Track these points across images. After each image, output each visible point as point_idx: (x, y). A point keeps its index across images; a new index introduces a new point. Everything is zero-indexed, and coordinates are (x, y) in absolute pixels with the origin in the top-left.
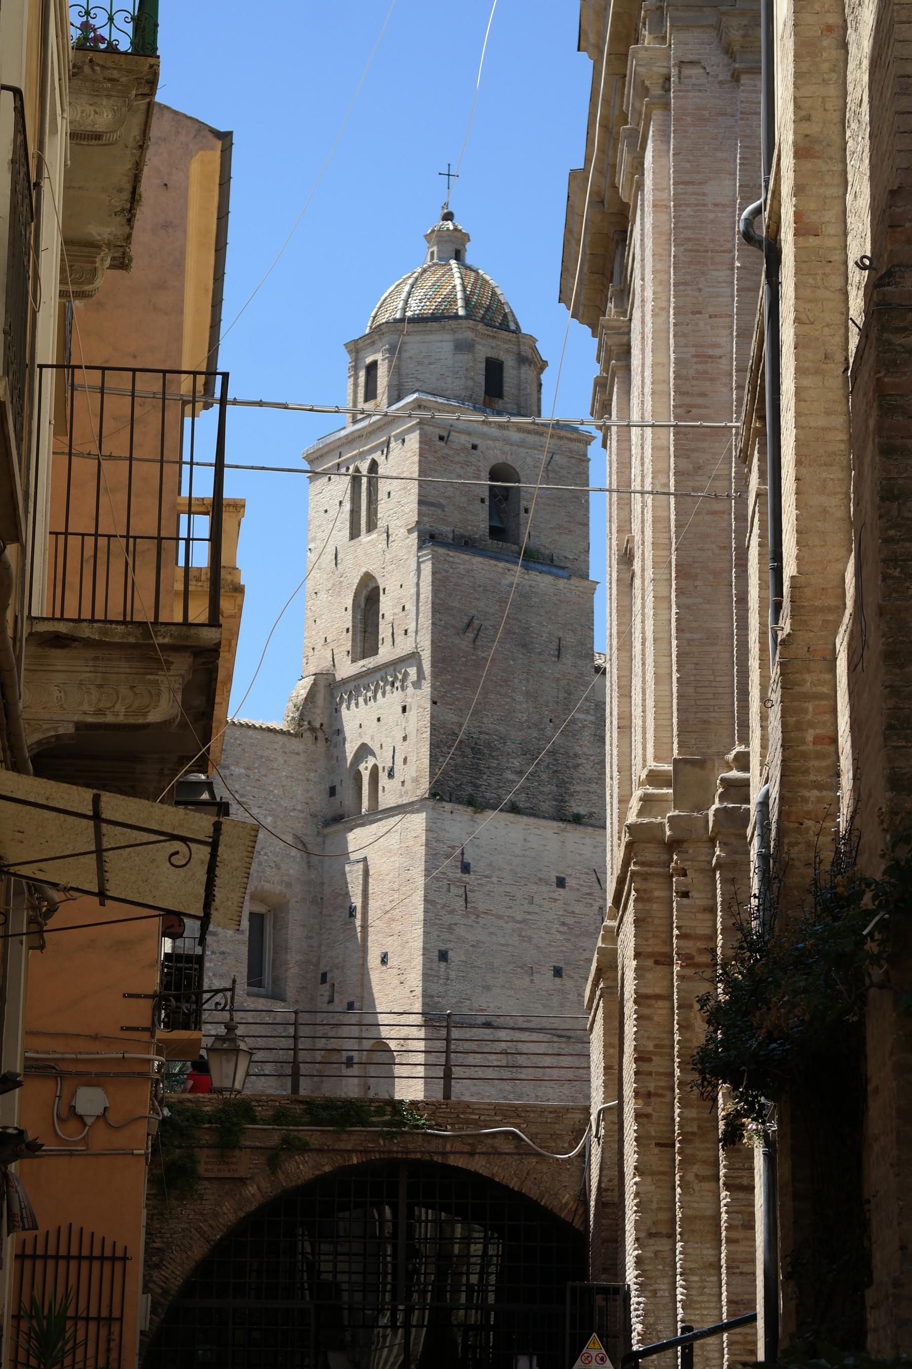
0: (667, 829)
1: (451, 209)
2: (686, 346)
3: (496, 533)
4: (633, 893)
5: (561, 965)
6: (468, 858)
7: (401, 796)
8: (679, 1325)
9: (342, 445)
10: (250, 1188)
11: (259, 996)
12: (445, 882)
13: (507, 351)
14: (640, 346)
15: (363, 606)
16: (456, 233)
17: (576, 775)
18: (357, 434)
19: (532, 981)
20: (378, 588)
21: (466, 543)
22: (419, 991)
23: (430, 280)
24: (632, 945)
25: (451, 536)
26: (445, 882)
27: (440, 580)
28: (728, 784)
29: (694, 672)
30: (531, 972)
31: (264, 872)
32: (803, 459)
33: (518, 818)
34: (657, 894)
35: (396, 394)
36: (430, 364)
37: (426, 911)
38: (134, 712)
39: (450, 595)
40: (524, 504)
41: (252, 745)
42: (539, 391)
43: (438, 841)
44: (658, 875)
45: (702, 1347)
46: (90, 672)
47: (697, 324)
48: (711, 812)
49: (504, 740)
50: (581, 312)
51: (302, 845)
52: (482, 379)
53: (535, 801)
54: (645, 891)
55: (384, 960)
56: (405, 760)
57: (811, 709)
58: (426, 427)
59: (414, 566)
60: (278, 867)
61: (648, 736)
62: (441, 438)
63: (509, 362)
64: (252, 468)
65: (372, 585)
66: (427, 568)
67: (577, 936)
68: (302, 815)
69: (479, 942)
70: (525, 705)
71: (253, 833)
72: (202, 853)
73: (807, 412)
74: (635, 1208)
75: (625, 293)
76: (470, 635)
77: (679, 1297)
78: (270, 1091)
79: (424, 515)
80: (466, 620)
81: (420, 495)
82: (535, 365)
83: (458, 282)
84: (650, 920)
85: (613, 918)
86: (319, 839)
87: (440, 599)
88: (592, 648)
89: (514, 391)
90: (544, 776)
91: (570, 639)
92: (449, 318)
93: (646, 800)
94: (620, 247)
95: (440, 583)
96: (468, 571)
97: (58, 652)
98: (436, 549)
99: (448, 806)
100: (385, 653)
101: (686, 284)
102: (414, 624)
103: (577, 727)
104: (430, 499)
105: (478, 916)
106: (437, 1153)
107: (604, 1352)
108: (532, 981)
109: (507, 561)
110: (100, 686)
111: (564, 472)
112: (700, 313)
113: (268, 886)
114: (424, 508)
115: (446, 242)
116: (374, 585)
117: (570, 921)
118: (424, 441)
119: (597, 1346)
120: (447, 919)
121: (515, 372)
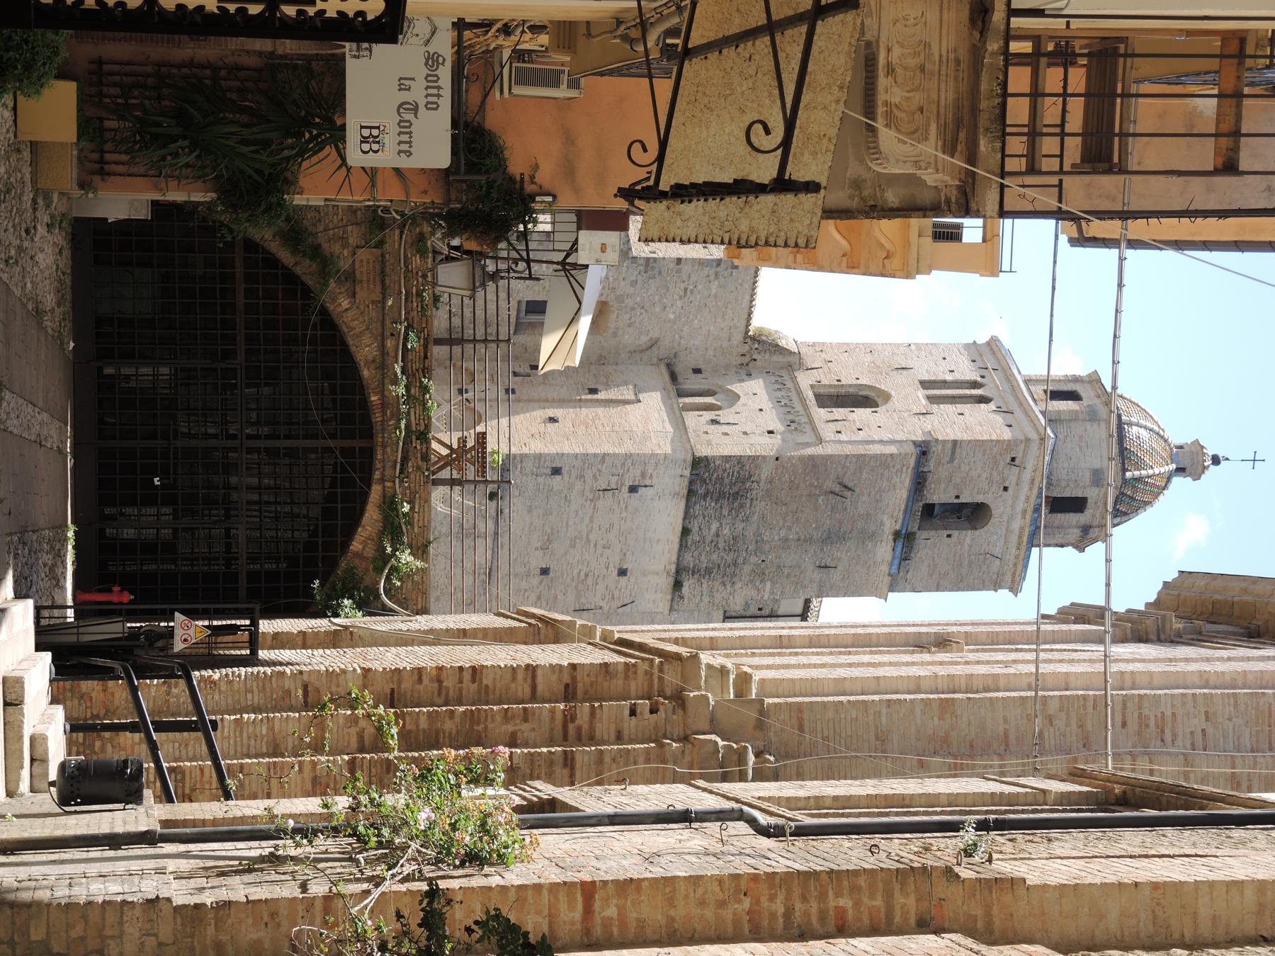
0: (695, 693)
1: (1223, 463)
2: (1173, 706)
3: (929, 510)
4: (633, 661)
5: (551, 574)
6: (642, 491)
7: (694, 431)
8: (219, 717)
9: (1004, 371)
10: (346, 302)
11: (518, 311)
12: (621, 472)
13: (1094, 516)
14: (1161, 656)
15: (860, 393)
16: (1200, 468)
17: (717, 584)
18: (1015, 384)
19: (537, 549)
20: (877, 406)
21: (919, 483)
22: (526, 450)
23: (1158, 446)
24: (583, 660)
25: (925, 470)
26: (621, 472)
27: (886, 461)
28: (741, 757)
29: (849, 718)
30: (544, 548)
31: (626, 313)
32: (1160, 891)
33: (679, 534)
34: (633, 684)
35: (1053, 421)
36: (1081, 448)
37: (595, 455)
38: (891, 112)
39: (873, 470)
40: (955, 533)
41: (736, 300)
42: (1057, 545)
43: (657, 464)
44: (651, 685)
45: (197, 739)
46: (941, 56)
47: (1195, 717)
48: (713, 737)
49: (746, 520)
50: (1172, 592)
51: (653, 344)
52: (1067, 494)
53: (693, 548)
54: (635, 673)
55: (553, 420)
56: (726, 434)
57: (875, 903)
58: (1023, 445)
59: (899, 437)
60: (630, 325)
61: (782, 671)
62: (1013, 459)
63: (1082, 518)
64: (1054, 280)
65: (879, 401)
66: (893, 449)
67: (576, 588)
68: (676, 345)
69: (570, 501)
70: (776, 538)
71: (802, 242)
72: (764, 171)
73: (1215, 894)
74: (331, 669)
75: (1197, 638)
76: (837, 488)
77: (246, 716)
78: (436, 323)
79: (943, 446)
80: (850, 485)
81: (961, 441)
82: (1081, 541)
83: (1157, 471)
84: (608, 678)
85: (604, 638)
86: (655, 361)
87: (869, 461)
88: (827, 596)
89: (1057, 523)
90: (715, 556)
91: (836, 576)
92: (1123, 464)
93: (723, 671)
94: (1242, 631)
95: (884, 462)
96: (894, 486)
97: (965, 14)
98: (914, 457)
99: (687, 473)
100: (821, 414)
101: (1236, 705)
102: (846, 439)
103: (757, 584)
104: (958, 450)
105: (592, 501)
106: (383, 474)
107: (193, 641)
108: (537, 549)
109: (904, 519)
110: (922, 69)
111: (985, 568)
112: (1207, 719)
113: (613, 316)
114: (950, 445)
115: (1192, 459)
116: (879, 403)
117: (590, 581)
118: (1009, 445)
119: (198, 635)
120: (589, 474)
121: (1074, 523)
